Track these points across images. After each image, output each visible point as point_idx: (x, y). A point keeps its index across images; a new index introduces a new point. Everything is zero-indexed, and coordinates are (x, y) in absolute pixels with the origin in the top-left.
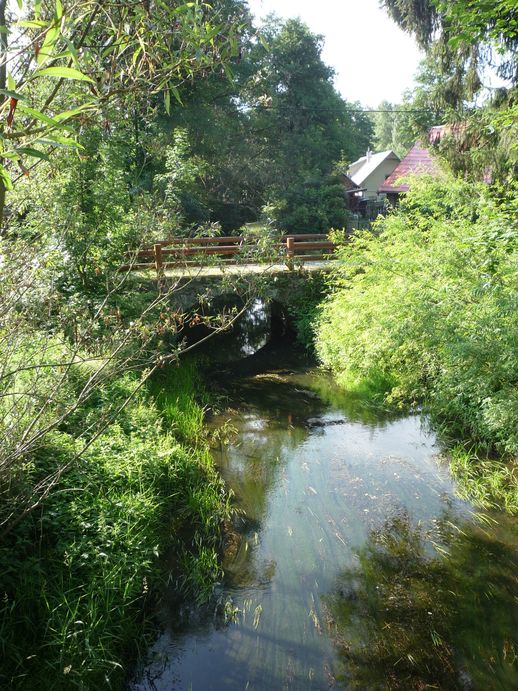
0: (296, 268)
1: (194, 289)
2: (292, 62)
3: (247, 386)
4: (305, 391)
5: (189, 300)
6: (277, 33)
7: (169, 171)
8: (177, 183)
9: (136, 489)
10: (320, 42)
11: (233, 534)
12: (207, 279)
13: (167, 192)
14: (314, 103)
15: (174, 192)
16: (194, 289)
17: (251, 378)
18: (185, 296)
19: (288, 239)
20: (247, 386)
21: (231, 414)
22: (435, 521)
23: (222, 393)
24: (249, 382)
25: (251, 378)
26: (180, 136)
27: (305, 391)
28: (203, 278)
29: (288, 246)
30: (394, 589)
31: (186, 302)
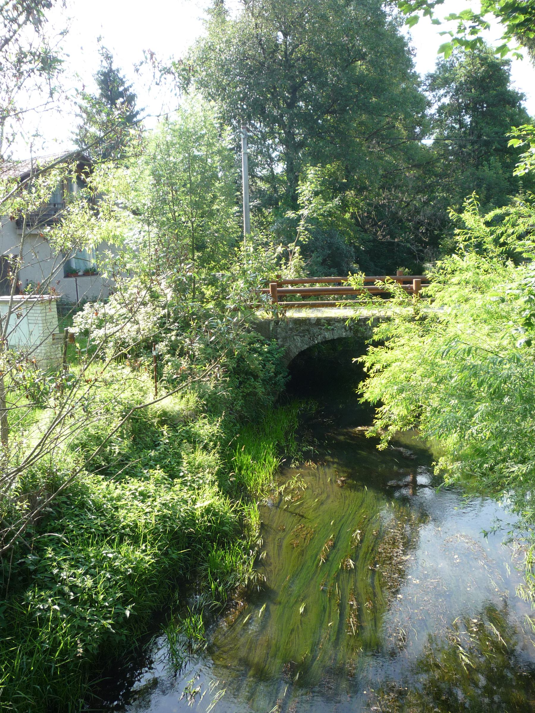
0: (280, 316)
1: (308, 330)
2: (473, 90)
3: (342, 438)
4: (401, 449)
5: (302, 342)
6: (460, 60)
7: (303, 207)
8: (310, 220)
9: (135, 540)
10: (506, 68)
11: (239, 602)
12: (323, 321)
13: (300, 229)
14: (496, 133)
15: (306, 229)
16: (308, 330)
17: (350, 430)
18: (298, 338)
19: (414, 280)
20: (342, 438)
21: (309, 468)
22: (475, 621)
23: (312, 443)
24: (347, 434)
25: (350, 430)
26: (312, 172)
27: (401, 449)
28: (318, 320)
29: (414, 288)
30: (383, 698)
31: (299, 344)
